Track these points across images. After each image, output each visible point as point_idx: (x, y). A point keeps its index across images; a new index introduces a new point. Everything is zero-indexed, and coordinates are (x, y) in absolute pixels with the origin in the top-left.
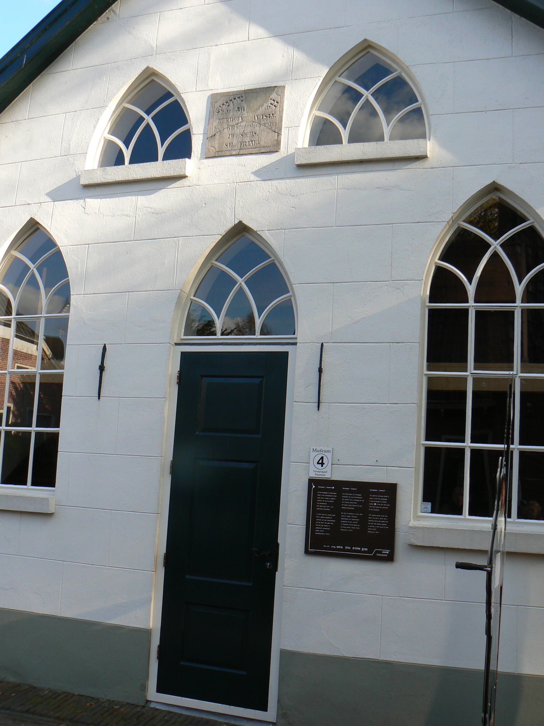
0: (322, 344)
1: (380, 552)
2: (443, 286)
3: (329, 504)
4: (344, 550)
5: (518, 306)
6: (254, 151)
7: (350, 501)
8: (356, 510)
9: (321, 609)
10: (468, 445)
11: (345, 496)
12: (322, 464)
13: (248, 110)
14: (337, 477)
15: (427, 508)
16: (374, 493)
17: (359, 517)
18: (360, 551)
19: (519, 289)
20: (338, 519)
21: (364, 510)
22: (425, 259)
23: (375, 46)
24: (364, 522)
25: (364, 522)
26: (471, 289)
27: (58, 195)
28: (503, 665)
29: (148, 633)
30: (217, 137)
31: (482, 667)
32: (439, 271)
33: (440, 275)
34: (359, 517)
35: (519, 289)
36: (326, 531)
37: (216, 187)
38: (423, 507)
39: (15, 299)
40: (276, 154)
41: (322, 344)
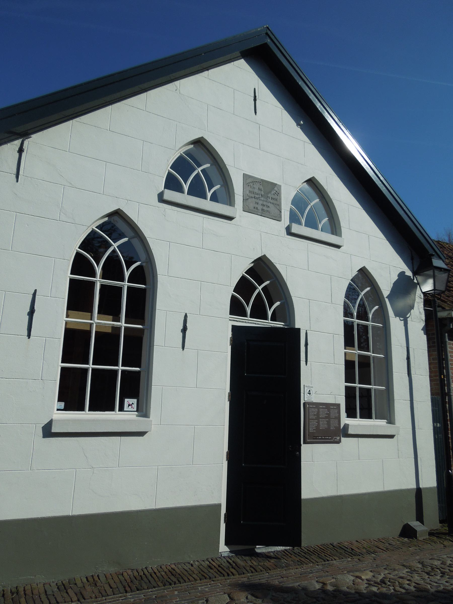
1: (336, 439)
2: (80, 265)
3: (315, 415)
5: (126, 284)
8: (326, 418)
9: (327, 472)
10: (120, 368)
11: (321, 410)
12: (310, 394)
14: (315, 401)
15: (61, 406)
16: (332, 408)
17: (327, 421)
19: (127, 274)
20: (318, 423)
21: (328, 417)
22: (73, 247)
23: (205, 143)
24: (329, 423)
25: (329, 423)
26: (99, 270)
29: (219, 506)
31: (414, 486)
32: (78, 255)
33: (78, 258)
34: (327, 421)
35: (127, 274)
36: (314, 430)
38: (59, 405)
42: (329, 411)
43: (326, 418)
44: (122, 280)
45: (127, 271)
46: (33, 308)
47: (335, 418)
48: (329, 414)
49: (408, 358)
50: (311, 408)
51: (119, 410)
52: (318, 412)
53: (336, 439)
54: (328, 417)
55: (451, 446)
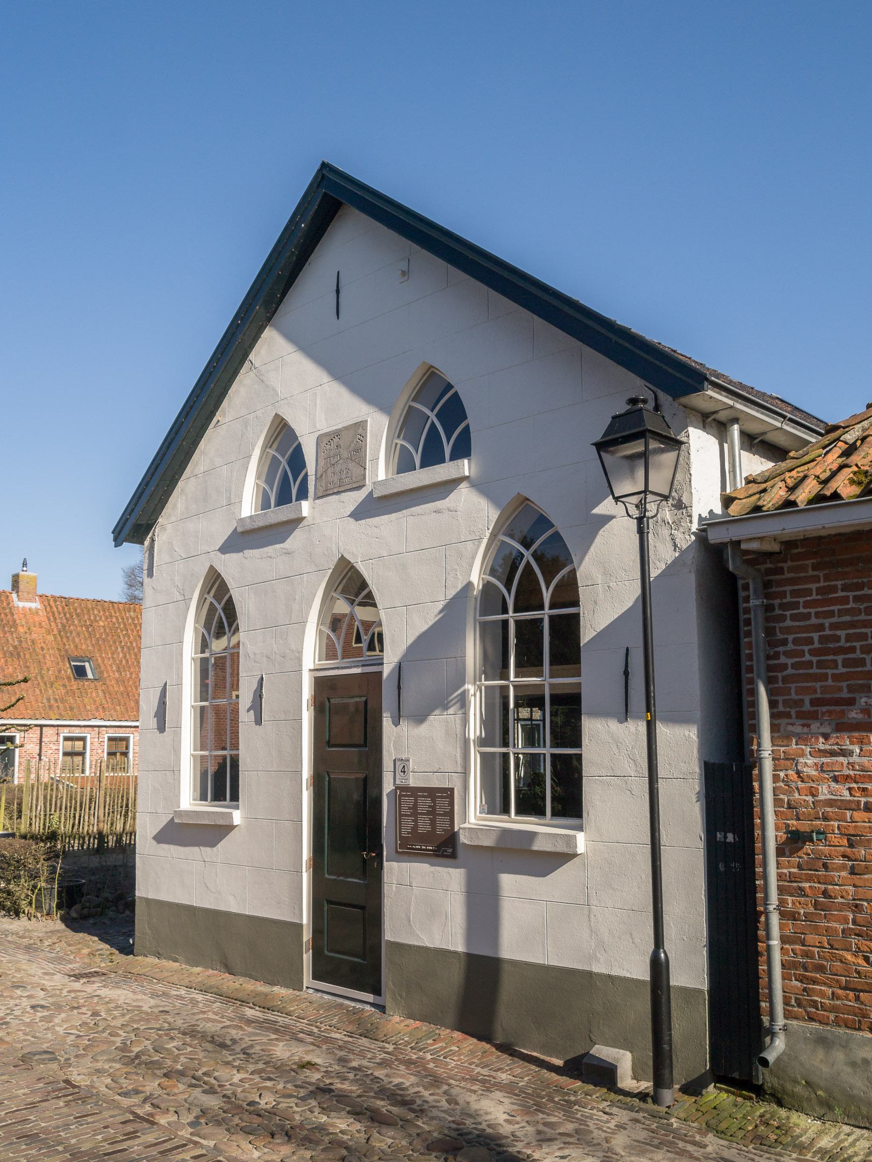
0: (627, 650)
1: (446, 851)
3: (410, 808)
4: (421, 849)
6: (349, 487)
7: (424, 804)
8: (428, 813)
11: (420, 800)
13: (347, 445)
16: (439, 797)
18: (421, 849)
19: (547, 596)
20: (416, 821)
24: (433, 823)
27: (226, 548)
28: (513, 946)
30: (324, 477)
35: (547, 596)
36: (409, 833)
37: (327, 524)
39: (338, 639)
40: (365, 488)
41: (627, 650)
42: (434, 801)
43: (428, 813)
44: (541, 607)
45: (547, 588)
46: (164, 703)
47: (445, 814)
48: (433, 807)
49: (399, 688)
50: (404, 796)
51: (231, 800)
52: (415, 805)
53: (446, 851)
54: (432, 812)
55: (349, 879)
